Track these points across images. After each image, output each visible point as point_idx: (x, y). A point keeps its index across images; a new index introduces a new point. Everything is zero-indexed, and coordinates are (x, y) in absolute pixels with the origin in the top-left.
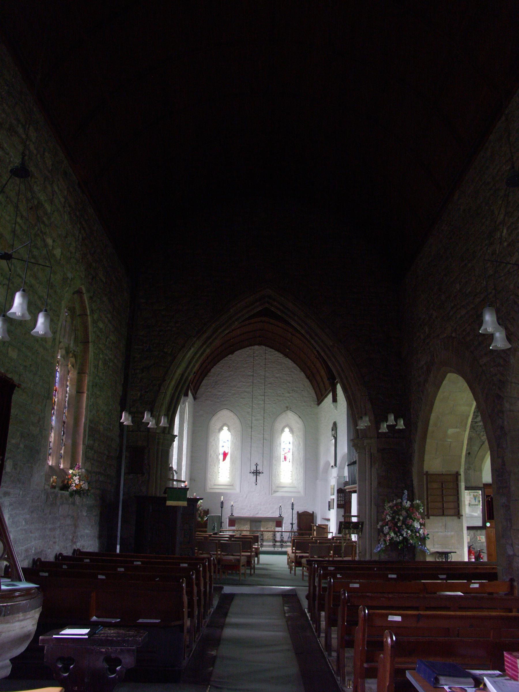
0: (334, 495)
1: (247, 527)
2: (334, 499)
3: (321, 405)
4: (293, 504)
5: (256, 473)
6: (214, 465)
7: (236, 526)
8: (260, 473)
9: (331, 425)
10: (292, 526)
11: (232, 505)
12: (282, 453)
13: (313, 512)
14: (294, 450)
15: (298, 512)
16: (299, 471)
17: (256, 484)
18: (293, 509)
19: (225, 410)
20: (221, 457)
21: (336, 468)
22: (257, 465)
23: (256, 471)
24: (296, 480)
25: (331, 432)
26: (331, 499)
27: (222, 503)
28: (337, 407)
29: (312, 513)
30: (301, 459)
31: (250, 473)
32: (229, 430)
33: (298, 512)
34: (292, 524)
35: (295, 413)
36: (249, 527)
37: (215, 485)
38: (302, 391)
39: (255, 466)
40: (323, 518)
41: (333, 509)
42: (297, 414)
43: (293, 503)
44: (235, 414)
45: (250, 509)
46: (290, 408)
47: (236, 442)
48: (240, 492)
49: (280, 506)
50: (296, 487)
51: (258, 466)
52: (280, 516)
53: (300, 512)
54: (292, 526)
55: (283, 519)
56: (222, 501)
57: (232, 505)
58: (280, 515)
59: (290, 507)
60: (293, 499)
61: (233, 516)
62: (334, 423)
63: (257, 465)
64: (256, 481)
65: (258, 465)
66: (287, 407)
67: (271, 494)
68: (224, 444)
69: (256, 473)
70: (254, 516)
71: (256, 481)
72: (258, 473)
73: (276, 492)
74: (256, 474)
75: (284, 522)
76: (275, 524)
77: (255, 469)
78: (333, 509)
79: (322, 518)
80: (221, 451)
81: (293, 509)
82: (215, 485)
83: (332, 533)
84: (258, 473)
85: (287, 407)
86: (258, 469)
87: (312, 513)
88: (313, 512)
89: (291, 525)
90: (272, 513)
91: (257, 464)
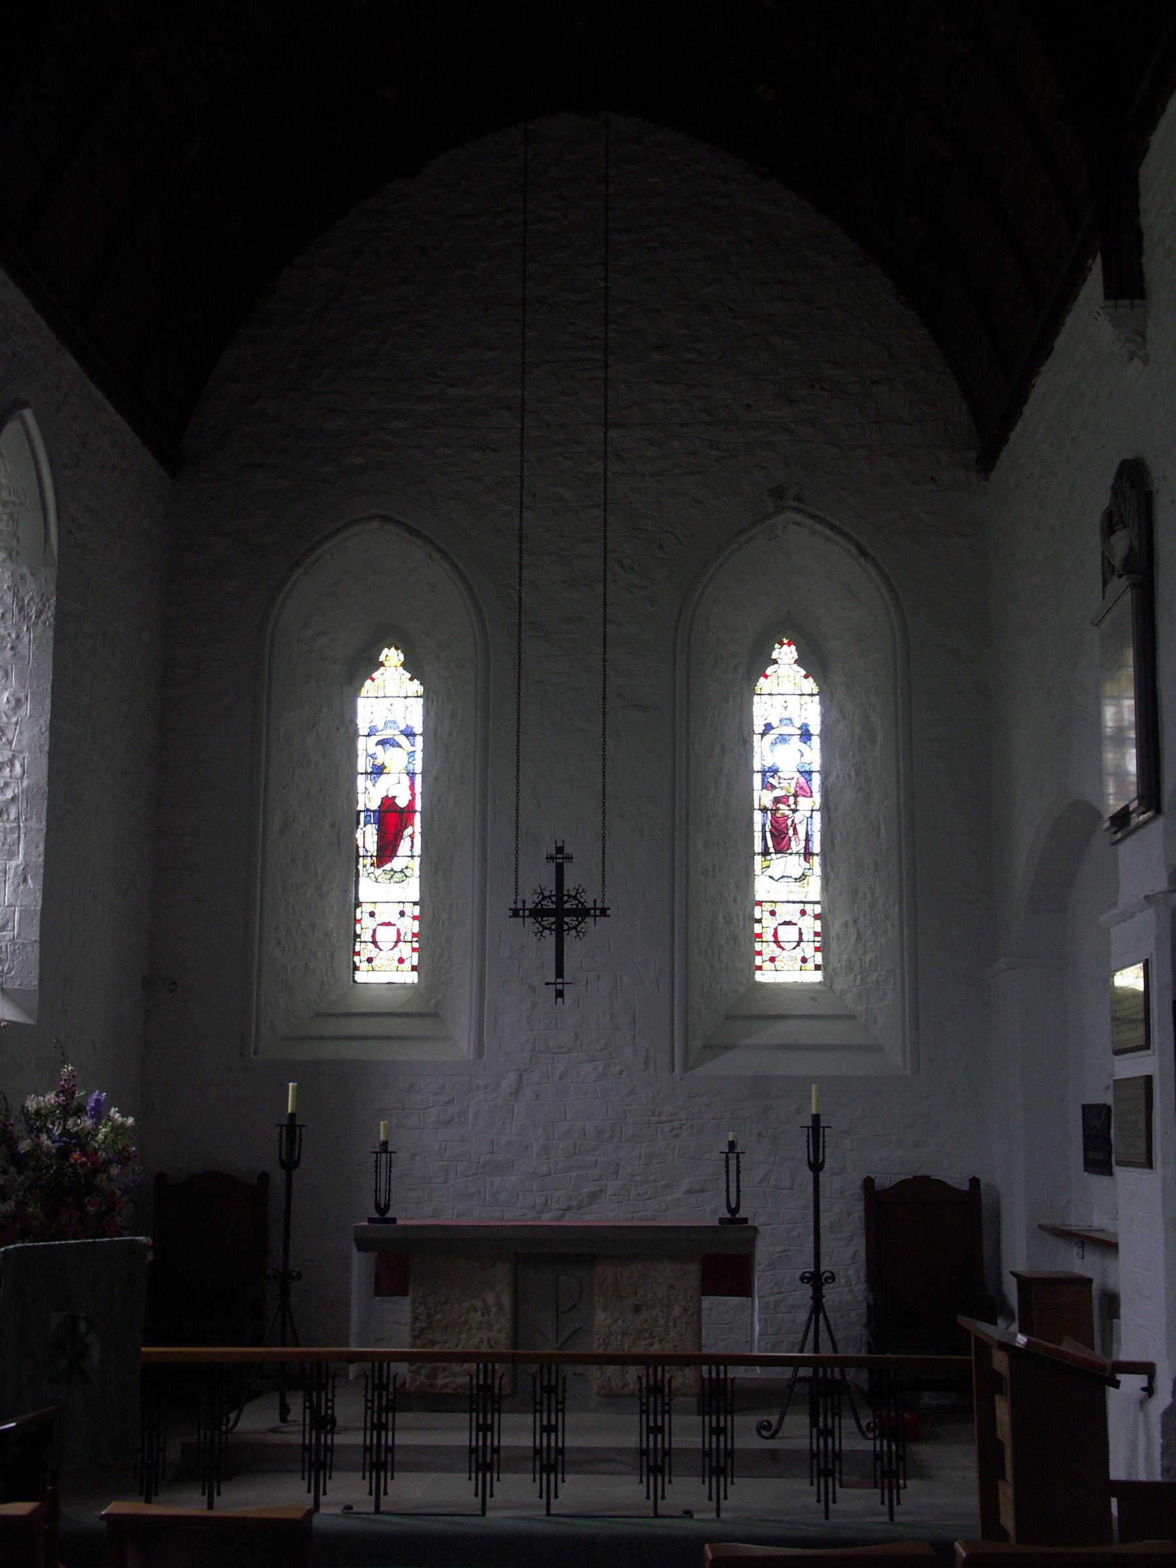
0: (1147, 1045)
1: (491, 1299)
2: (1149, 1080)
3: (1005, 459)
4: (816, 1127)
5: (560, 913)
6: (319, 888)
7: (410, 1294)
8: (582, 913)
9: (1099, 496)
10: (817, 1298)
11: (385, 1144)
12: (761, 797)
13: (974, 1182)
14: (833, 778)
15: (868, 1183)
16: (872, 906)
17: (560, 994)
18: (816, 1167)
19: (375, 524)
20: (368, 837)
21: (1160, 822)
22: (560, 858)
23: (560, 902)
24: (850, 966)
25: (1097, 539)
26: (1120, 1085)
27: (292, 1128)
28: (1142, 335)
29: (965, 1187)
30: (883, 830)
31: (515, 913)
32: (412, 666)
33: (868, 1183)
34: (816, 1280)
35: (833, 527)
36: (506, 1301)
37: (318, 1015)
38: (876, 382)
39: (552, 867)
40: (1046, 1222)
41: (1149, 1164)
42: (841, 533)
43: (816, 1118)
44: (438, 549)
45: (543, 1169)
46: (799, 499)
47: (450, 734)
48: (480, 1053)
49: (732, 1145)
50: (851, 1017)
51: (568, 867)
52: (734, 1219)
53: (886, 1179)
54: (817, 1298)
55: (751, 1242)
56: (292, 1116)
57: (385, 1144)
58: (733, 1211)
59: (801, 1150)
60: (814, 1087)
61: (394, 1220)
62: (1120, 473)
63: (560, 858)
64: (560, 972)
65: (550, 858)
66: (778, 493)
67: (686, 1067)
68: (386, 756)
69: (560, 913)
70: (570, 1220)
71: (560, 972)
72: (549, 913)
73: (714, 1048)
74: (560, 923)
75: (763, 1251)
76: (692, 1273)
77: (550, 887)
78: (1149, 1164)
79: (1041, 1227)
80: (369, 796)
81: (816, 1167)
82: (318, 1015)
83: (1147, 1369)
84: (549, 913)
85: (778, 493)
86: (569, 885)
87: (965, 1187)
88: (974, 1182)
89: (807, 1290)
90: (690, 1192)
91: (560, 850)
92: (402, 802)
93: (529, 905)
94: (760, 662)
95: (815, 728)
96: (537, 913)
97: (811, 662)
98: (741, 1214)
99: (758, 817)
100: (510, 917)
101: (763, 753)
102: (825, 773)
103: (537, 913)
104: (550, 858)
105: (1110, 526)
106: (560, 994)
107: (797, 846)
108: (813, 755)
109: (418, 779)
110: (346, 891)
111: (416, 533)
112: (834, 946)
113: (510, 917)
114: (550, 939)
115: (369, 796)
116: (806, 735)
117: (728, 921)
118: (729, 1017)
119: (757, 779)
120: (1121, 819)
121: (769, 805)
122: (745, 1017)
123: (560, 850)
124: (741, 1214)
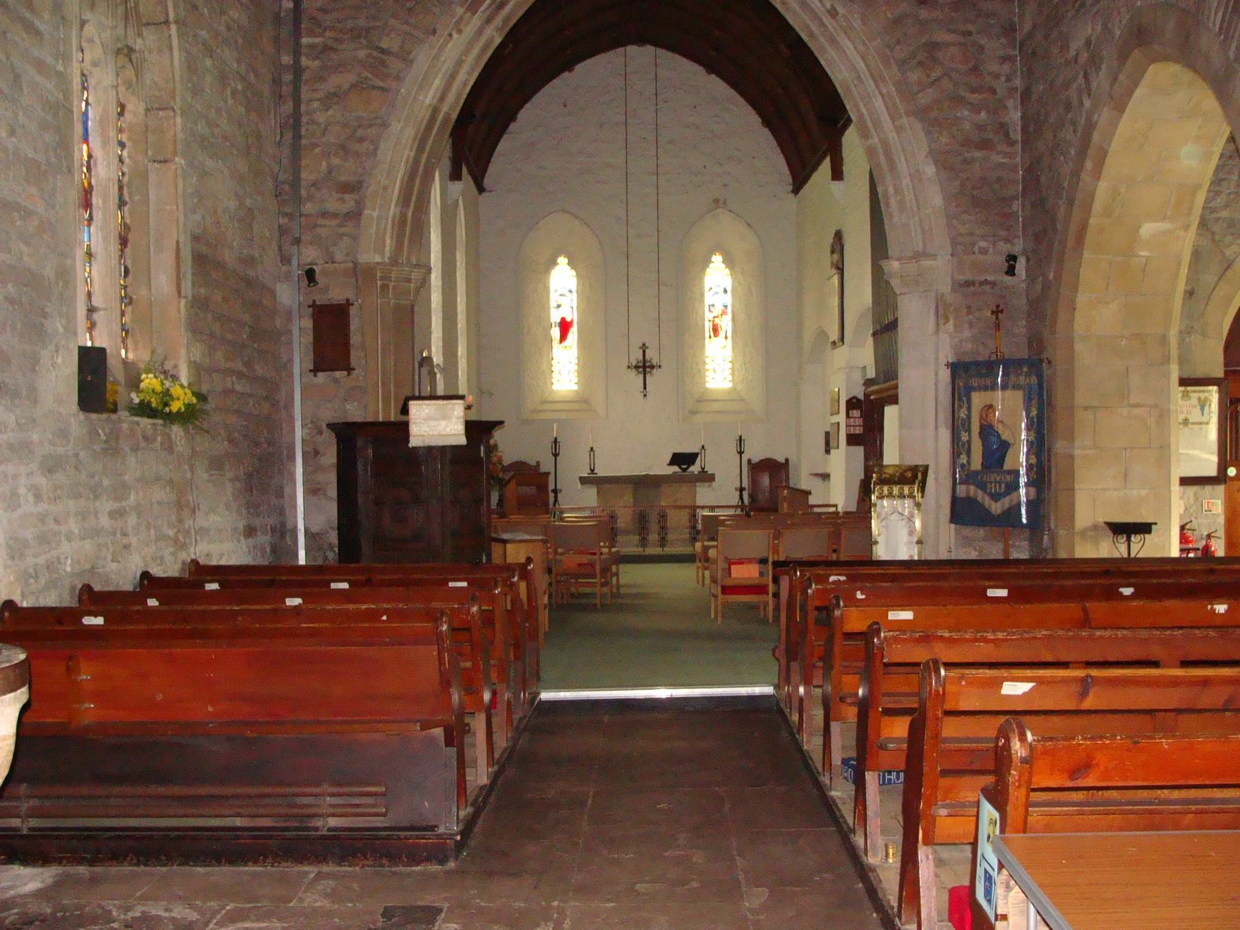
2: (838, 423)
5: (644, 367)
8: (652, 367)
9: (829, 239)
12: (708, 316)
17: (645, 395)
20: (556, 332)
22: (644, 348)
31: (629, 367)
39: (641, 351)
63: (644, 348)
64: (645, 388)
65: (640, 348)
66: (716, 201)
68: (561, 301)
71: (645, 388)
73: (693, 413)
77: (641, 358)
78: (838, 447)
79: (811, 474)
80: (555, 317)
87: (784, 461)
88: (787, 460)
91: (644, 345)
92: (568, 319)
93: (634, 364)
94: (707, 262)
95: (729, 289)
96: (636, 367)
97: (729, 262)
98: (706, 470)
99: (707, 323)
100: (1156, 524)
101: (708, 299)
102: (733, 306)
103: (636, 367)
104: (640, 348)
105: (833, 252)
106: (645, 395)
107: (722, 334)
108: (728, 299)
109: (575, 309)
110: (549, 355)
111: (576, 217)
112: (736, 373)
113: (1156, 524)
114: (641, 376)
115: (555, 317)
116: (725, 291)
117: (697, 364)
118: (697, 401)
119: (707, 308)
120: (834, 343)
121: (711, 319)
122: (706, 401)
123: (644, 345)
124: (706, 470)
